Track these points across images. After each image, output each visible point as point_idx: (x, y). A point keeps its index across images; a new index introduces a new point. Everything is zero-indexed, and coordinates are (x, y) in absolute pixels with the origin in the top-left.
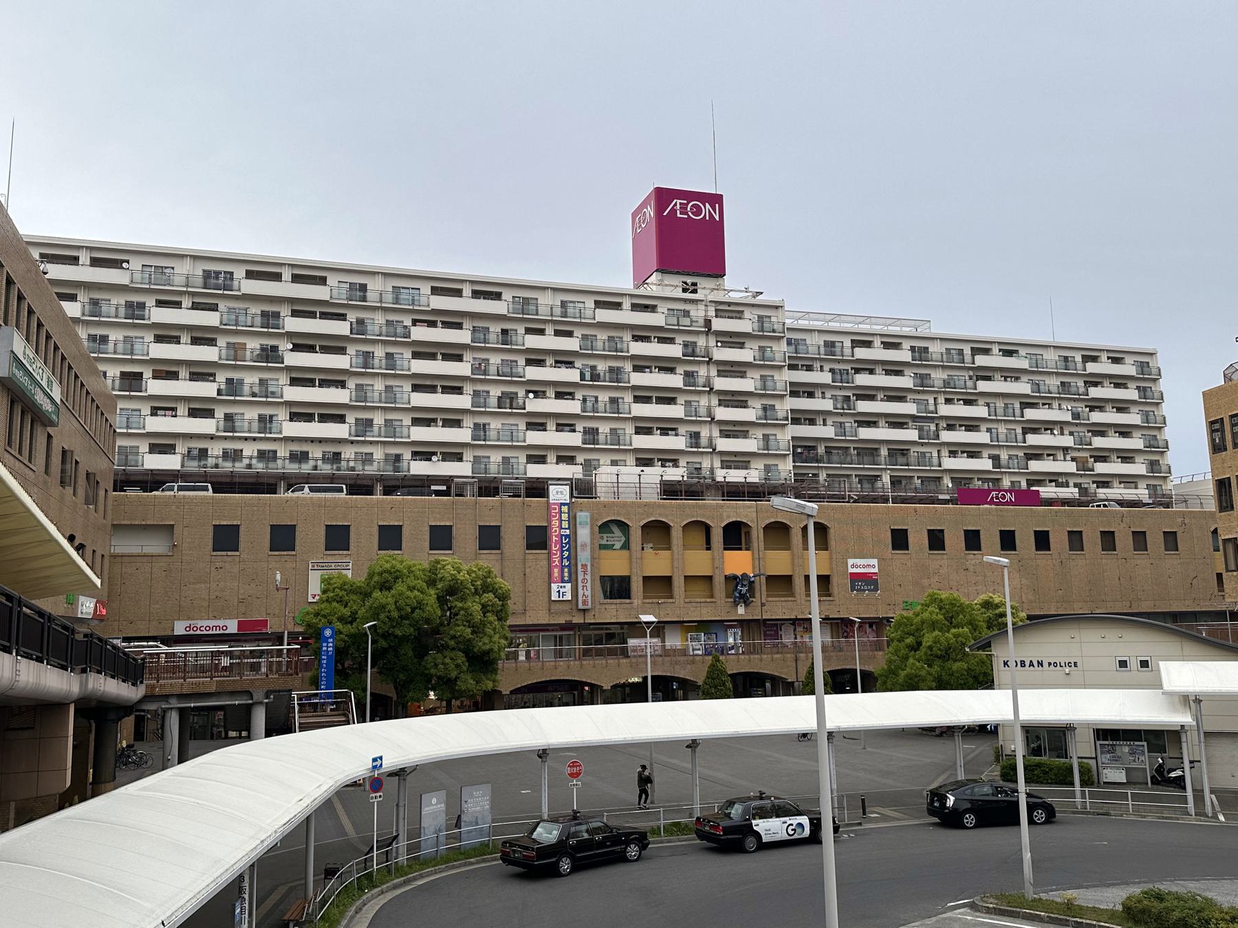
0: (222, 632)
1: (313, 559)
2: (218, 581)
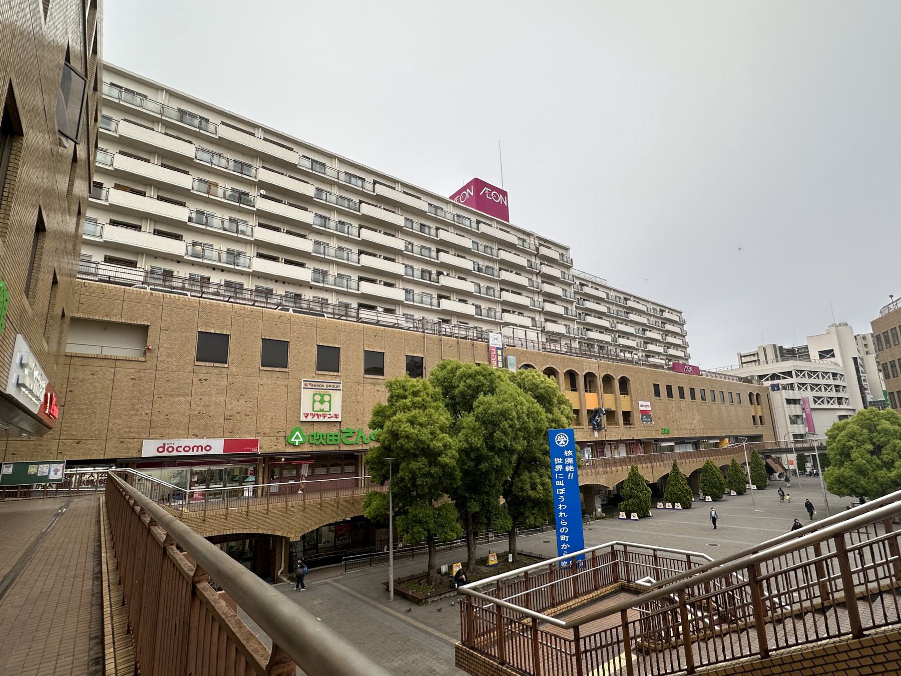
0: (204, 452)
1: (305, 378)
2: (202, 394)
